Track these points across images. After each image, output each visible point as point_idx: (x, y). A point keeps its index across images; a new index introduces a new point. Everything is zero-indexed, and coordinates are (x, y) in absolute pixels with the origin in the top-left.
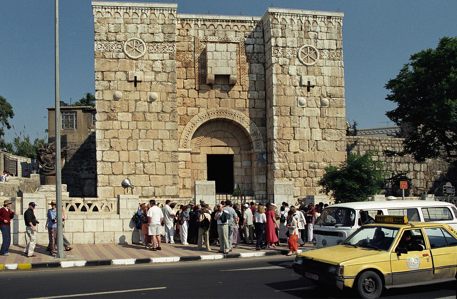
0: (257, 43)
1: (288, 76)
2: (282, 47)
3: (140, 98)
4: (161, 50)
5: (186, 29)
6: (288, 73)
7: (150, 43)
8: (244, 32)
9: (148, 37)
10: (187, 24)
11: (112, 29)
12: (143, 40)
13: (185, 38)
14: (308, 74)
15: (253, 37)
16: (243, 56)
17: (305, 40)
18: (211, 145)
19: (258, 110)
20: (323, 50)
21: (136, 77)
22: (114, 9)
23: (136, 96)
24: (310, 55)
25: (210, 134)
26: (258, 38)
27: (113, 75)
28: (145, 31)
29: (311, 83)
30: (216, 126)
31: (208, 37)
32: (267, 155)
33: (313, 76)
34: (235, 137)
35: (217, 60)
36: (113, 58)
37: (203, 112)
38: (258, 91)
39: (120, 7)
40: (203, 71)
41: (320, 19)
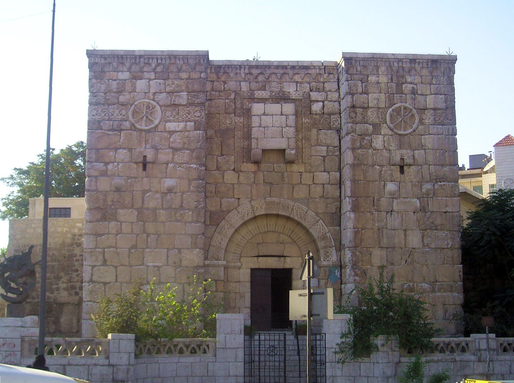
0: (329, 99)
4: (183, 117)
5: (223, 81)
8: (309, 83)
10: (224, 73)
12: (158, 103)
13: (222, 94)
18: (257, 255)
19: (330, 201)
24: (404, 119)
25: (256, 236)
26: (330, 91)
28: (160, 90)
30: (266, 225)
31: (255, 92)
32: (341, 270)
34: (295, 242)
35: (266, 128)
38: (328, 172)
39: (126, 56)
40: (246, 143)
41: (420, 65)
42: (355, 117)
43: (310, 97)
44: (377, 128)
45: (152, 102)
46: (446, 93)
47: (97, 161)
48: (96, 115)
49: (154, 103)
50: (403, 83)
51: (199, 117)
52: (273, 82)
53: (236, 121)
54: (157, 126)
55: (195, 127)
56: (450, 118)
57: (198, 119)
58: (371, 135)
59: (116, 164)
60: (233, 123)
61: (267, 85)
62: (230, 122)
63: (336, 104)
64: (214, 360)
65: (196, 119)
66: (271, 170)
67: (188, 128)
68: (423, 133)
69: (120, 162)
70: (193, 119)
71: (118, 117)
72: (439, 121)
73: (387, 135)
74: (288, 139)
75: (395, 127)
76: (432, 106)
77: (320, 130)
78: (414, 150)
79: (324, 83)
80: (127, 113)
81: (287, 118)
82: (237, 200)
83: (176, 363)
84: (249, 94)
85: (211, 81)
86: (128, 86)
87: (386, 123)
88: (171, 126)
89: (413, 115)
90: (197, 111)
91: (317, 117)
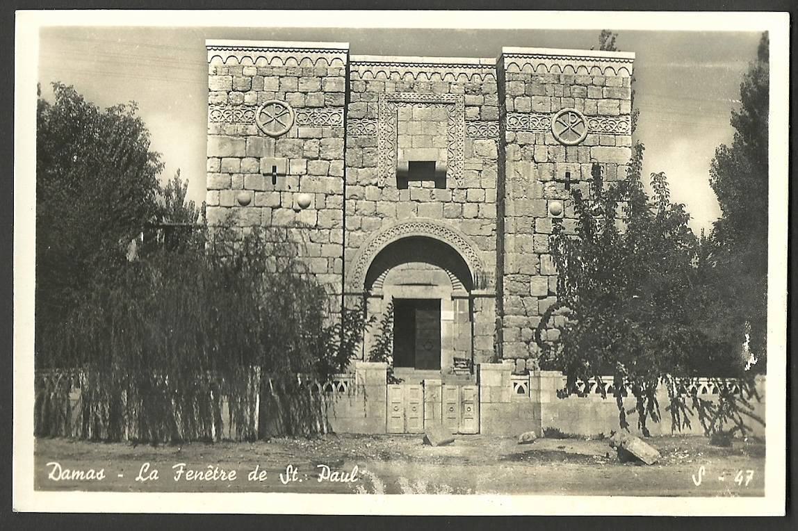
1: (532, 163)
3: (281, 203)
7: (302, 108)
9: (297, 99)
23: (274, 199)
37: (388, 224)
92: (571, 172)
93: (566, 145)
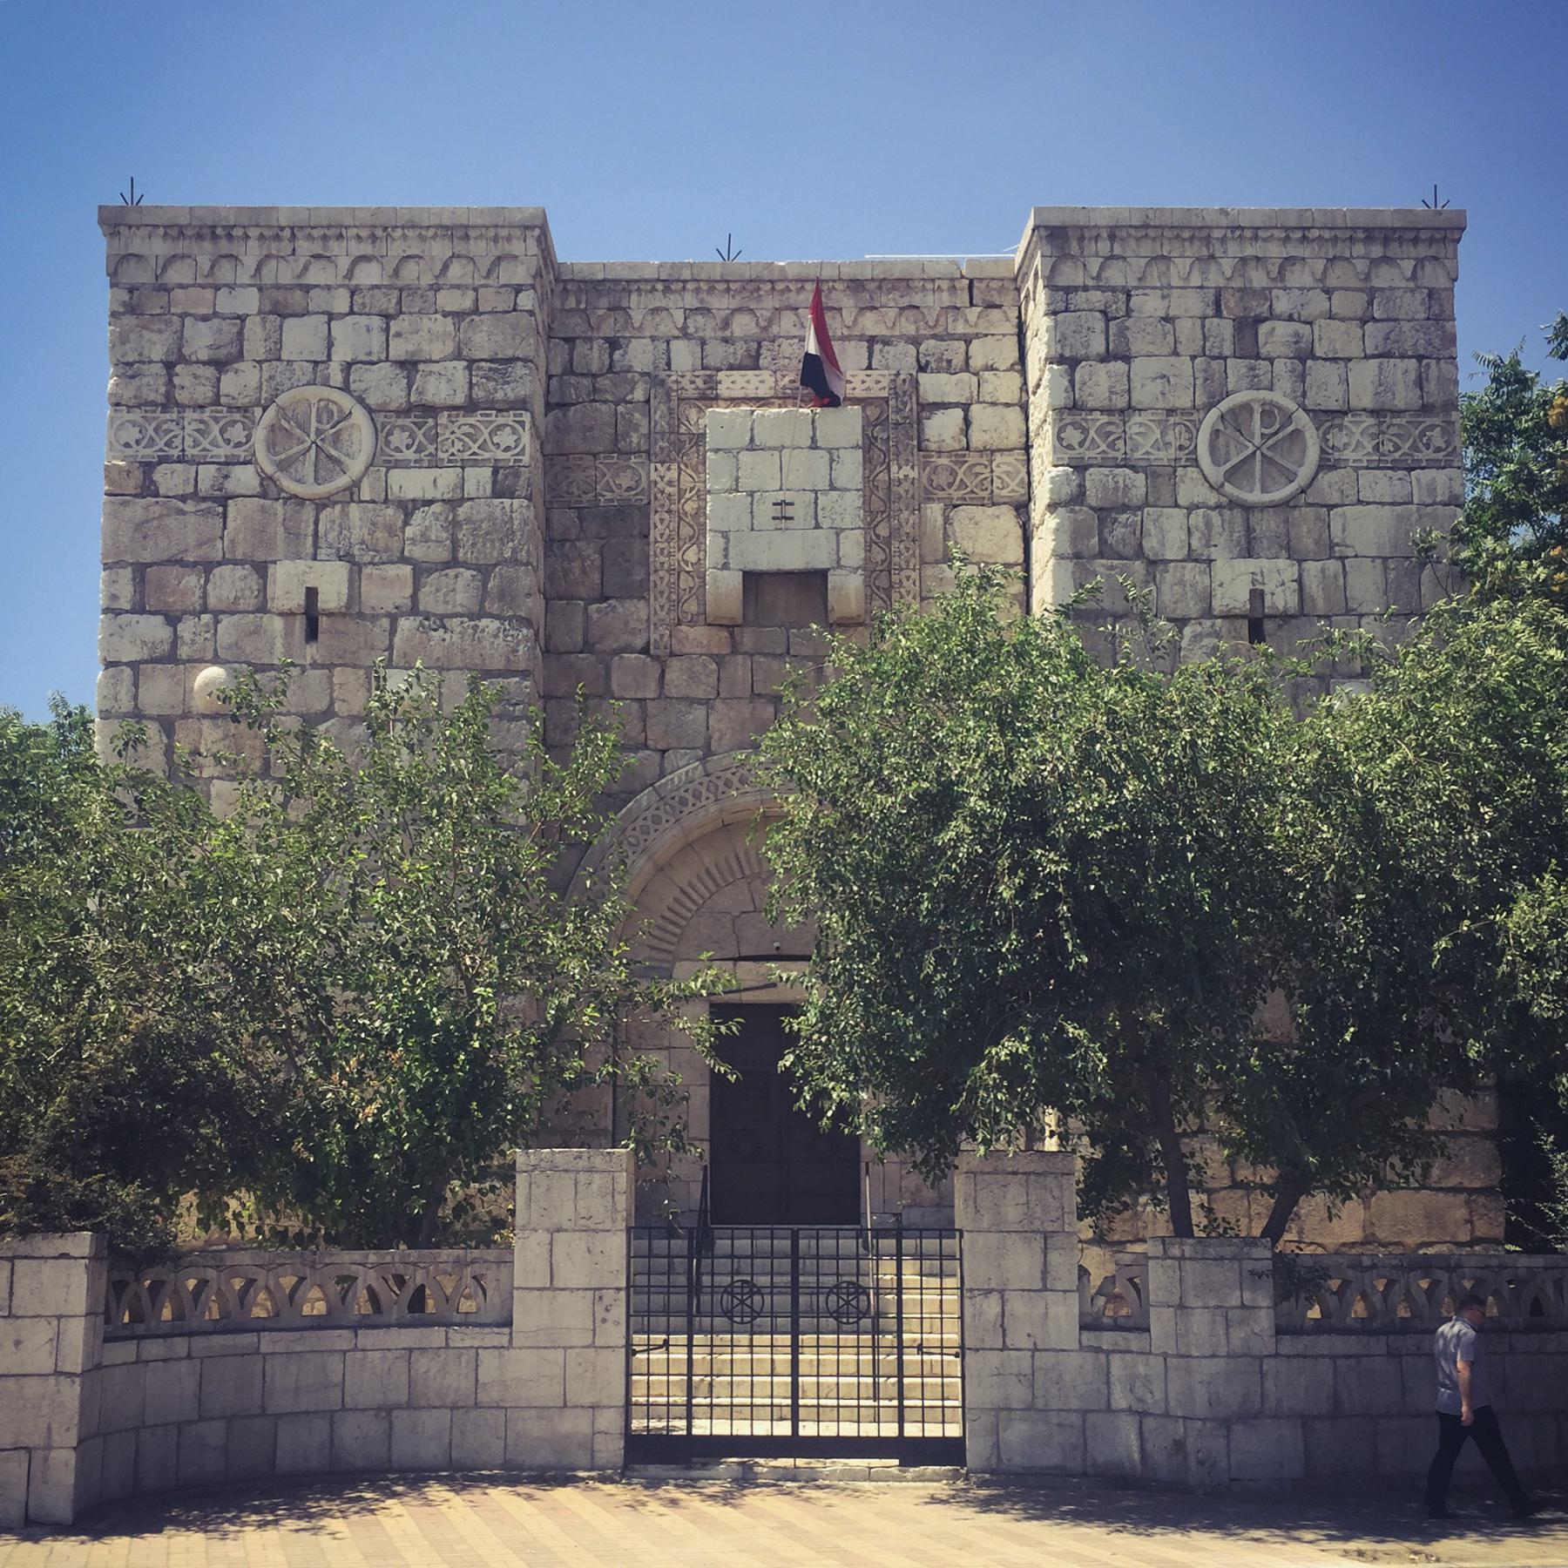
2: (1108, 411)
5: (607, 339)
6: (1139, 553)
8: (916, 341)
11: (201, 340)
12: (361, 400)
14: (1249, 552)
15: (966, 367)
16: (906, 470)
17: (1236, 368)
20: (1345, 413)
21: (312, 593)
22: (214, 236)
27: (192, 581)
28: (370, 354)
29: (1268, 598)
33: (1282, 563)
35: (757, 495)
36: (195, 496)
42: (1081, 444)
43: (917, 389)
44: (1161, 478)
45: (338, 396)
46: (1422, 352)
47: (139, 609)
48: (138, 442)
49: (346, 402)
50: (1259, 320)
51: (508, 449)
52: (787, 338)
53: (654, 476)
54: (356, 484)
55: (494, 483)
56: (1439, 442)
57: (507, 455)
58: (1140, 508)
59: (206, 618)
60: (644, 484)
61: (763, 351)
62: (633, 484)
63: (1015, 415)
64: (505, 1341)
65: (500, 455)
66: (779, 651)
67: (470, 490)
68: (1335, 498)
69: (223, 612)
70: (486, 455)
71: (216, 451)
72: (1397, 455)
73: (1198, 507)
74: (838, 535)
75: (1230, 476)
76: (1367, 402)
77: (955, 506)
78: (1300, 562)
79: (968, 342)
80: (248, 438)
81: (832, 460)
82: (657, 757)
83: (344, 1352)
84: (700, 383)
85: (566, 340)
86: (255, 345)
87: (1195, 463)
88: (411, 483)
89: (1297, 433)
90: (500, 427)
91: (944, 461)
92: (1267, 589)
93: (1248, 508)
